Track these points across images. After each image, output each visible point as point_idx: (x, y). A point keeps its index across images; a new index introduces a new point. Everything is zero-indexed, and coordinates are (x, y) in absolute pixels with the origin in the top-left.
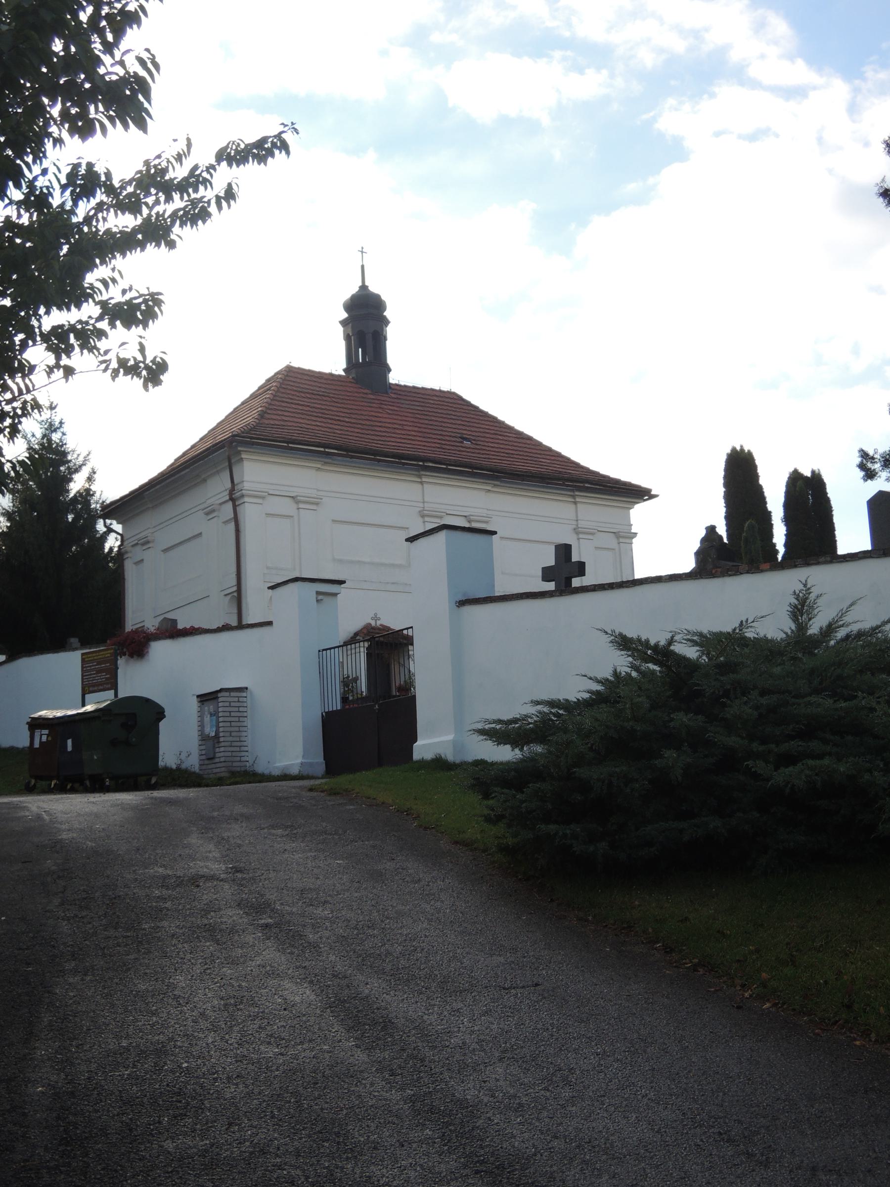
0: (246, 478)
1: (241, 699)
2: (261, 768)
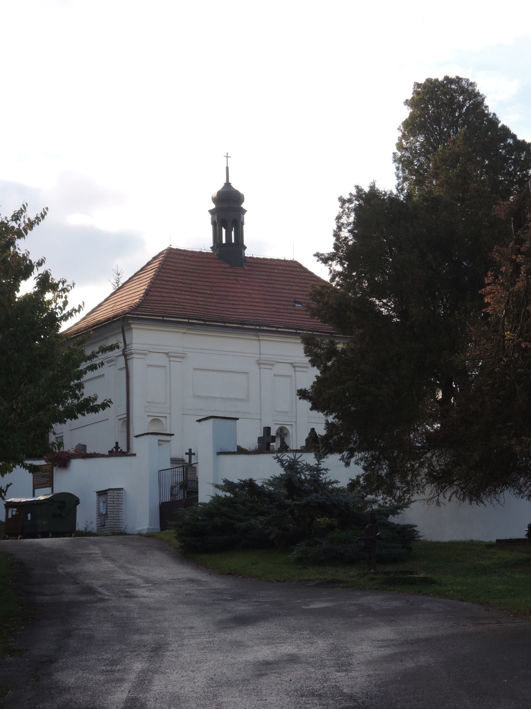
0: (134, 341)
1: (119, 494)
2: (128, 531)
